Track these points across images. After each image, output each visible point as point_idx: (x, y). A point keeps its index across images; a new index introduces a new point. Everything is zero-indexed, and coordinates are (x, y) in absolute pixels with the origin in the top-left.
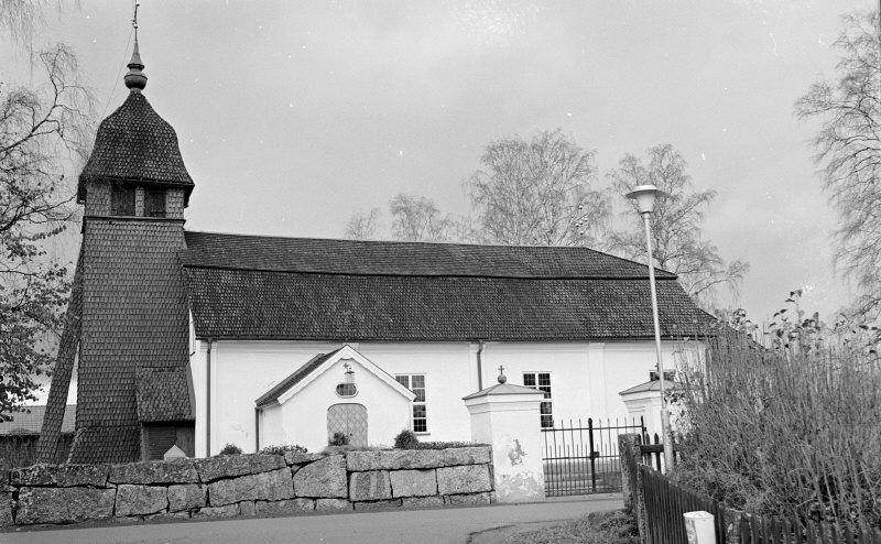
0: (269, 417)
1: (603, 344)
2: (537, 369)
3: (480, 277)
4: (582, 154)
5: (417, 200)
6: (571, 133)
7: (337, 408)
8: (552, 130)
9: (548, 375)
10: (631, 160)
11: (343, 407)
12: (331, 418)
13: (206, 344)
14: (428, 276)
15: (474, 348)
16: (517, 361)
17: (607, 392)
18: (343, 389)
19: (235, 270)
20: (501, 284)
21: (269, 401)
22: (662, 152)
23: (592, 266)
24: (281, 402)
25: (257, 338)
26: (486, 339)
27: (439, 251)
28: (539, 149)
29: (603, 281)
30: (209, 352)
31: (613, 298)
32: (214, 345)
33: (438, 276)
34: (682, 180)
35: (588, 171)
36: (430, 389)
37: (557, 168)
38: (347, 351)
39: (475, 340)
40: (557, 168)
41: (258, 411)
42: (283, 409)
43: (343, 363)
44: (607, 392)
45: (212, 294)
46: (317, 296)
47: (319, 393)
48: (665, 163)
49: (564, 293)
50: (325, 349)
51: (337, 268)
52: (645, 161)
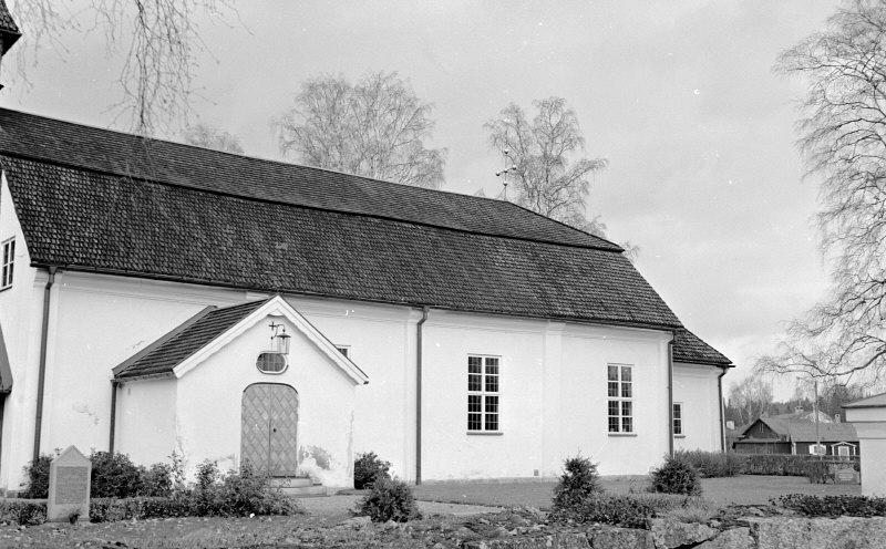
0: (138, 397)
1: (562, 325)
2: (483, 350)
3: (407, 222)
4: (418, 105)
5: (220, 133)
6: (409, 79)
7: (256, 389)
8: (386, 74)
9: (497, 360)
10: (515, 111)
11: (266, 388)
12: (248, 403)
13: (44, 275)
14: (343, 213)
15: (415, 315)
16: (453, 342)
17: (558, 401)
18: (269, 361)
19: (81, 169)
20: (433, 234)
21: (156, 364)
22: (554, 105)
23: (531, 226)
24: (178, 375)
25: (127, 273)
26: (432, 306)
27: (342, 184)
28: (372, 94)
29: (545, 245)
30: (48, 287)
31: (562, 269)
32: (58, 277)
33: (355, 214)
34: (571, 143)
35: (420, 127)
36: (502, 367)
37: (390, 118)
38: (277, 305)
39: (419, 306)
40: (390, 118)
41: (116, 385)
42: (180, 386)
43: (270, 322)
44: (558, 401)
45: (49, 197)
46: (203, 221)
47: (226, 366)
48: (555, 120)
49: (504, 255)
50: (225, 300)
51: (223, 187)
52: (531, 115)
